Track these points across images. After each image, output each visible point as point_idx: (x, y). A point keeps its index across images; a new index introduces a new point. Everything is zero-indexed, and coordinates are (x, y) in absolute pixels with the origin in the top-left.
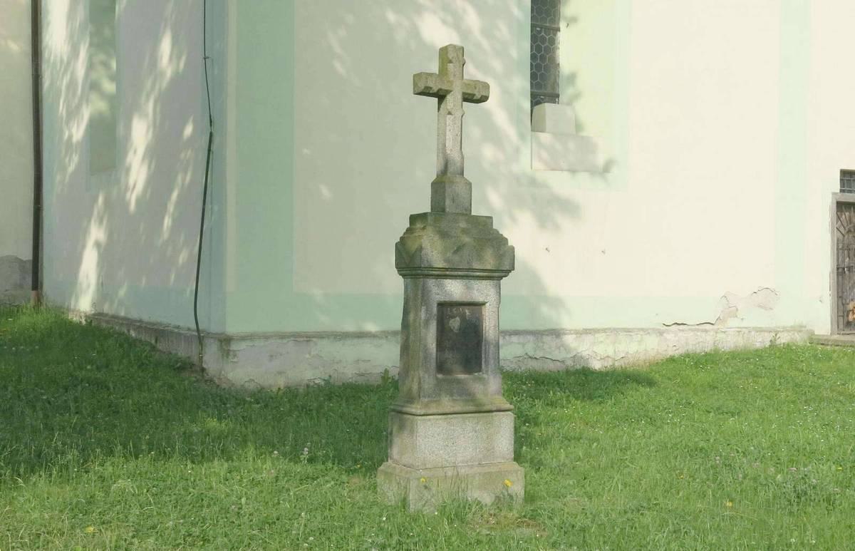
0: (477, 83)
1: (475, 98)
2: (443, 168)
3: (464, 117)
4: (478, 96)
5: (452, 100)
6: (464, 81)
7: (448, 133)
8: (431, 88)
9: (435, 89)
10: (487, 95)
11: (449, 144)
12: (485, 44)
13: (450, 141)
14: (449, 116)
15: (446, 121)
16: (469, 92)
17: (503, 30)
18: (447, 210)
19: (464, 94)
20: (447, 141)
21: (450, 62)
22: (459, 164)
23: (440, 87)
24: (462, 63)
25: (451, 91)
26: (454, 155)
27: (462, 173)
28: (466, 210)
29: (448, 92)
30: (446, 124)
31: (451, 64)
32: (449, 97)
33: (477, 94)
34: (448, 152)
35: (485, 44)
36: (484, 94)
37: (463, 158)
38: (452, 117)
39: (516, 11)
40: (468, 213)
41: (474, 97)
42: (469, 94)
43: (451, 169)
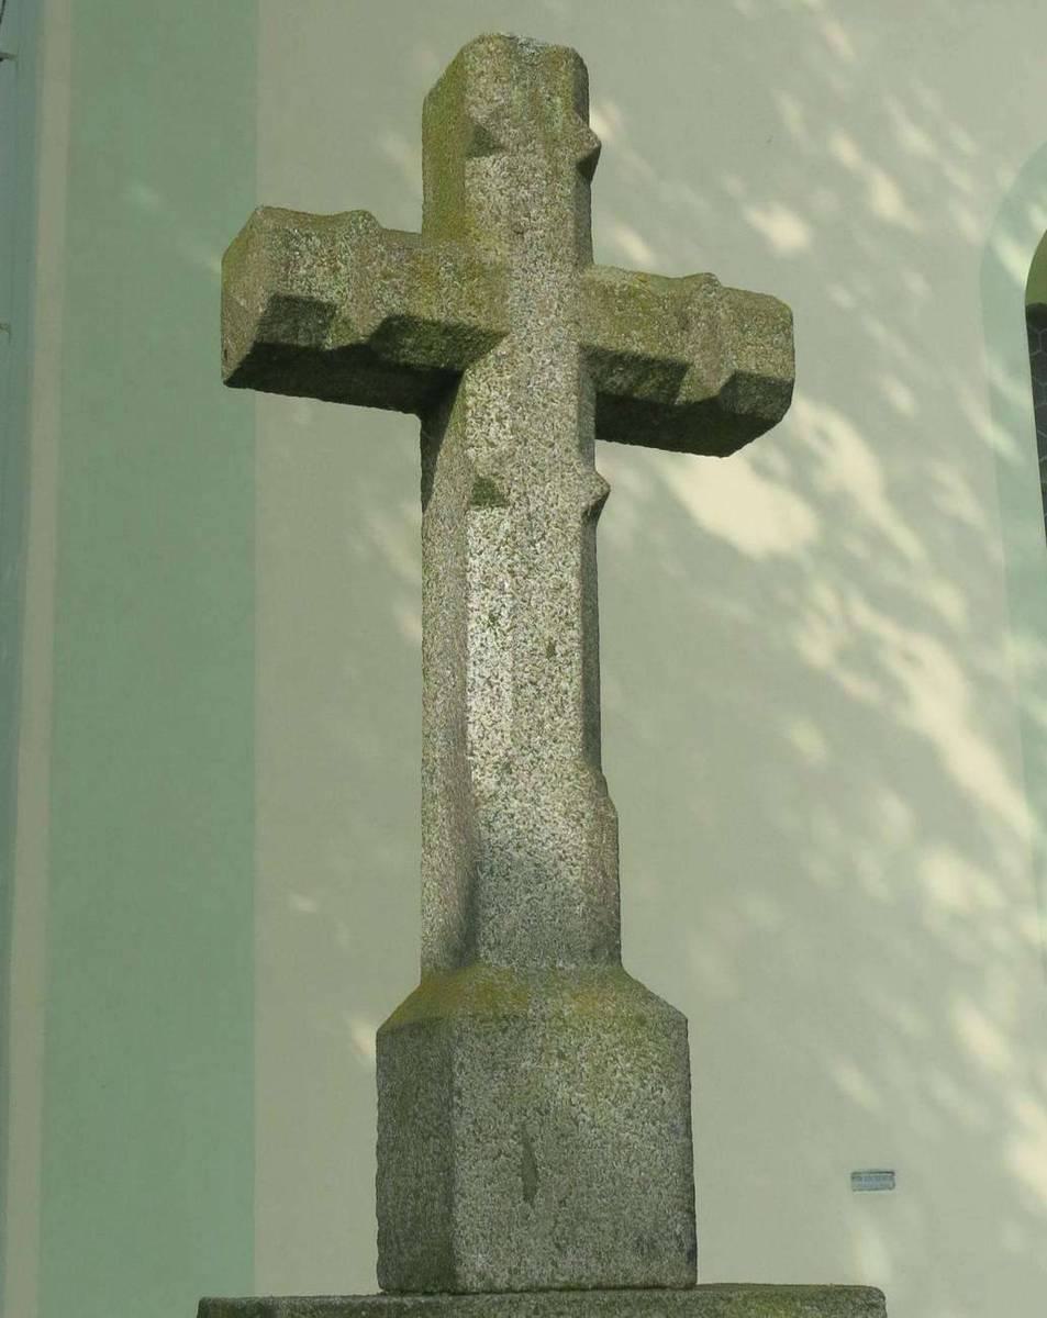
0: (685, 299)
1: (687, 393)
2: (455, 909)
3: (605, 521)
4: (705, 380)
5: (518, 402)
6: (599, 272)
7: (479, 637)
8: (325, 311)
9: (359, 322)
10: (770, 370)
11: (490, 719)
12: (907, 541)
13: (497, 699)
14: (480, 517)
15: (462, 549)
16: (636, 344)
17: (962, 502)
18: (475, 1263)
19: (596, 360)
20: (476, 703)
21: (484, 143)
22: (573, 876)
23: (396, 305)
24: (569, 156)
25: (495, 337)
26: (539, 813)
27: (607, 942)
28: (646, 1247)
29: (471, 344)
30: (462, 574)
31: (487, 163)
32: (481, 388)
33: (699, 363)
34: (486, 781)
35: (907, 541)
36: (750, 365)
37: (606, 825)
38: (502, 521)
39: (996, 437)
40: (664, 1269)
41: (680, 396)
42: (645, 365)
43: (504, 919)
